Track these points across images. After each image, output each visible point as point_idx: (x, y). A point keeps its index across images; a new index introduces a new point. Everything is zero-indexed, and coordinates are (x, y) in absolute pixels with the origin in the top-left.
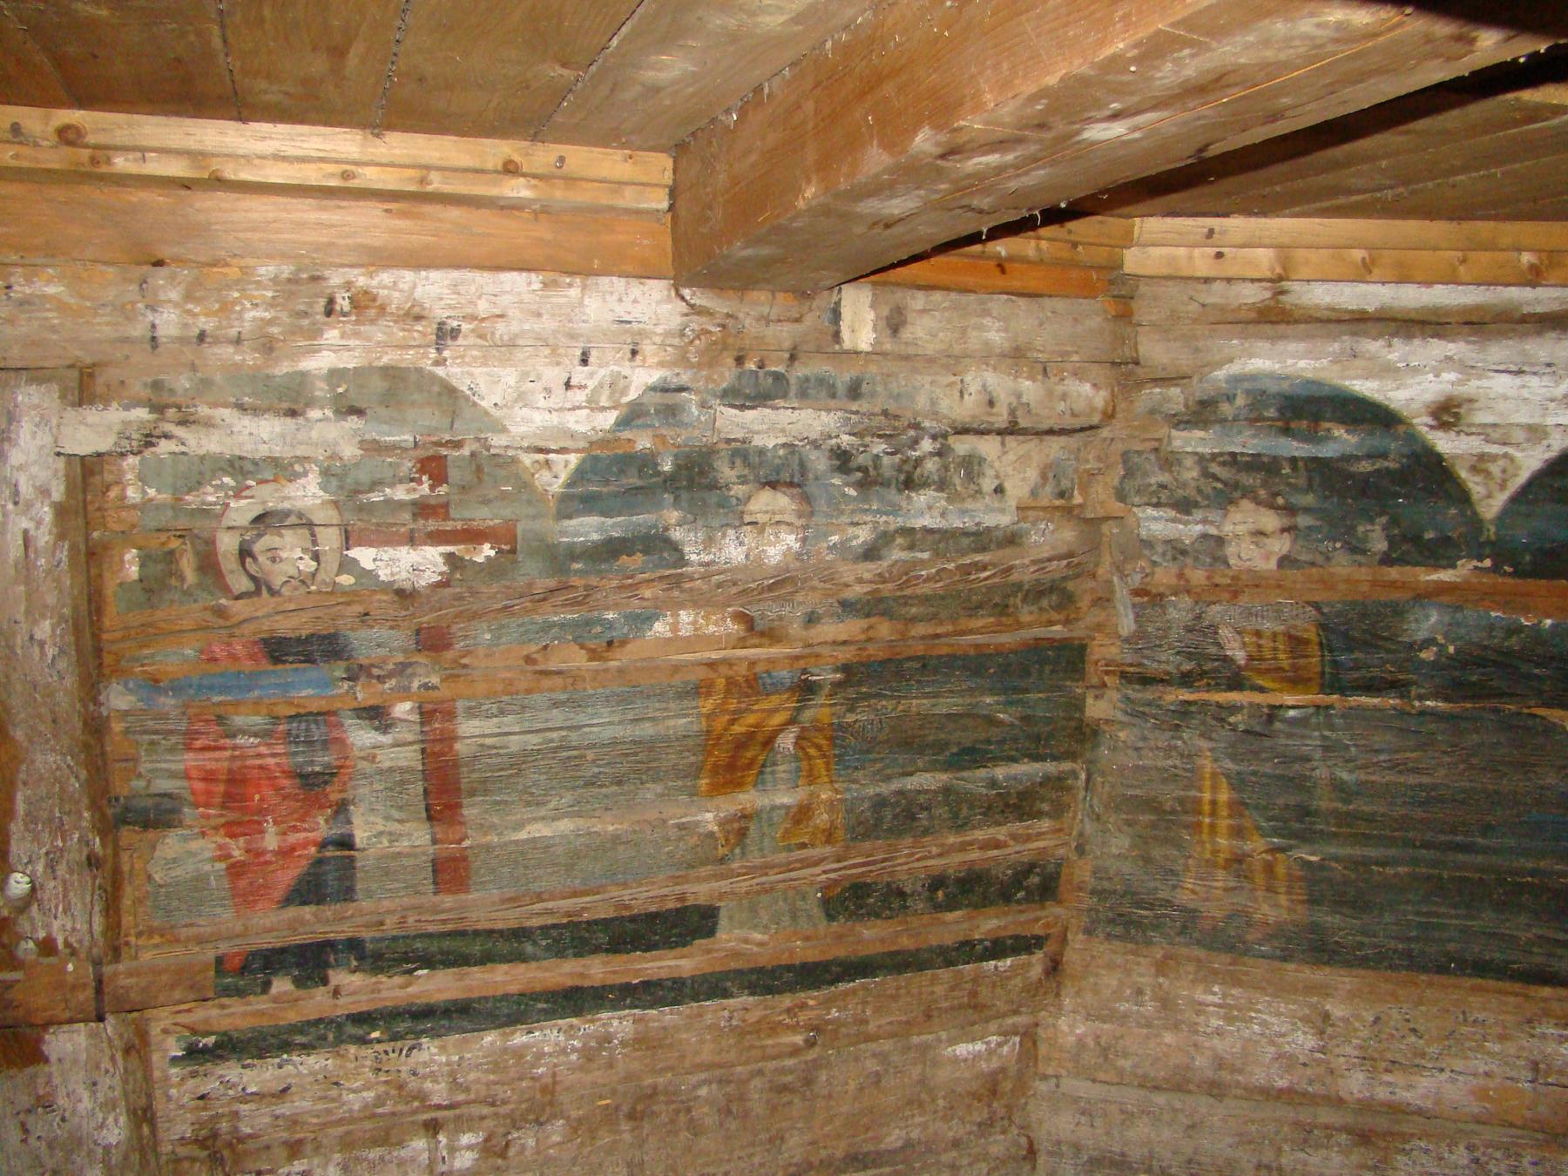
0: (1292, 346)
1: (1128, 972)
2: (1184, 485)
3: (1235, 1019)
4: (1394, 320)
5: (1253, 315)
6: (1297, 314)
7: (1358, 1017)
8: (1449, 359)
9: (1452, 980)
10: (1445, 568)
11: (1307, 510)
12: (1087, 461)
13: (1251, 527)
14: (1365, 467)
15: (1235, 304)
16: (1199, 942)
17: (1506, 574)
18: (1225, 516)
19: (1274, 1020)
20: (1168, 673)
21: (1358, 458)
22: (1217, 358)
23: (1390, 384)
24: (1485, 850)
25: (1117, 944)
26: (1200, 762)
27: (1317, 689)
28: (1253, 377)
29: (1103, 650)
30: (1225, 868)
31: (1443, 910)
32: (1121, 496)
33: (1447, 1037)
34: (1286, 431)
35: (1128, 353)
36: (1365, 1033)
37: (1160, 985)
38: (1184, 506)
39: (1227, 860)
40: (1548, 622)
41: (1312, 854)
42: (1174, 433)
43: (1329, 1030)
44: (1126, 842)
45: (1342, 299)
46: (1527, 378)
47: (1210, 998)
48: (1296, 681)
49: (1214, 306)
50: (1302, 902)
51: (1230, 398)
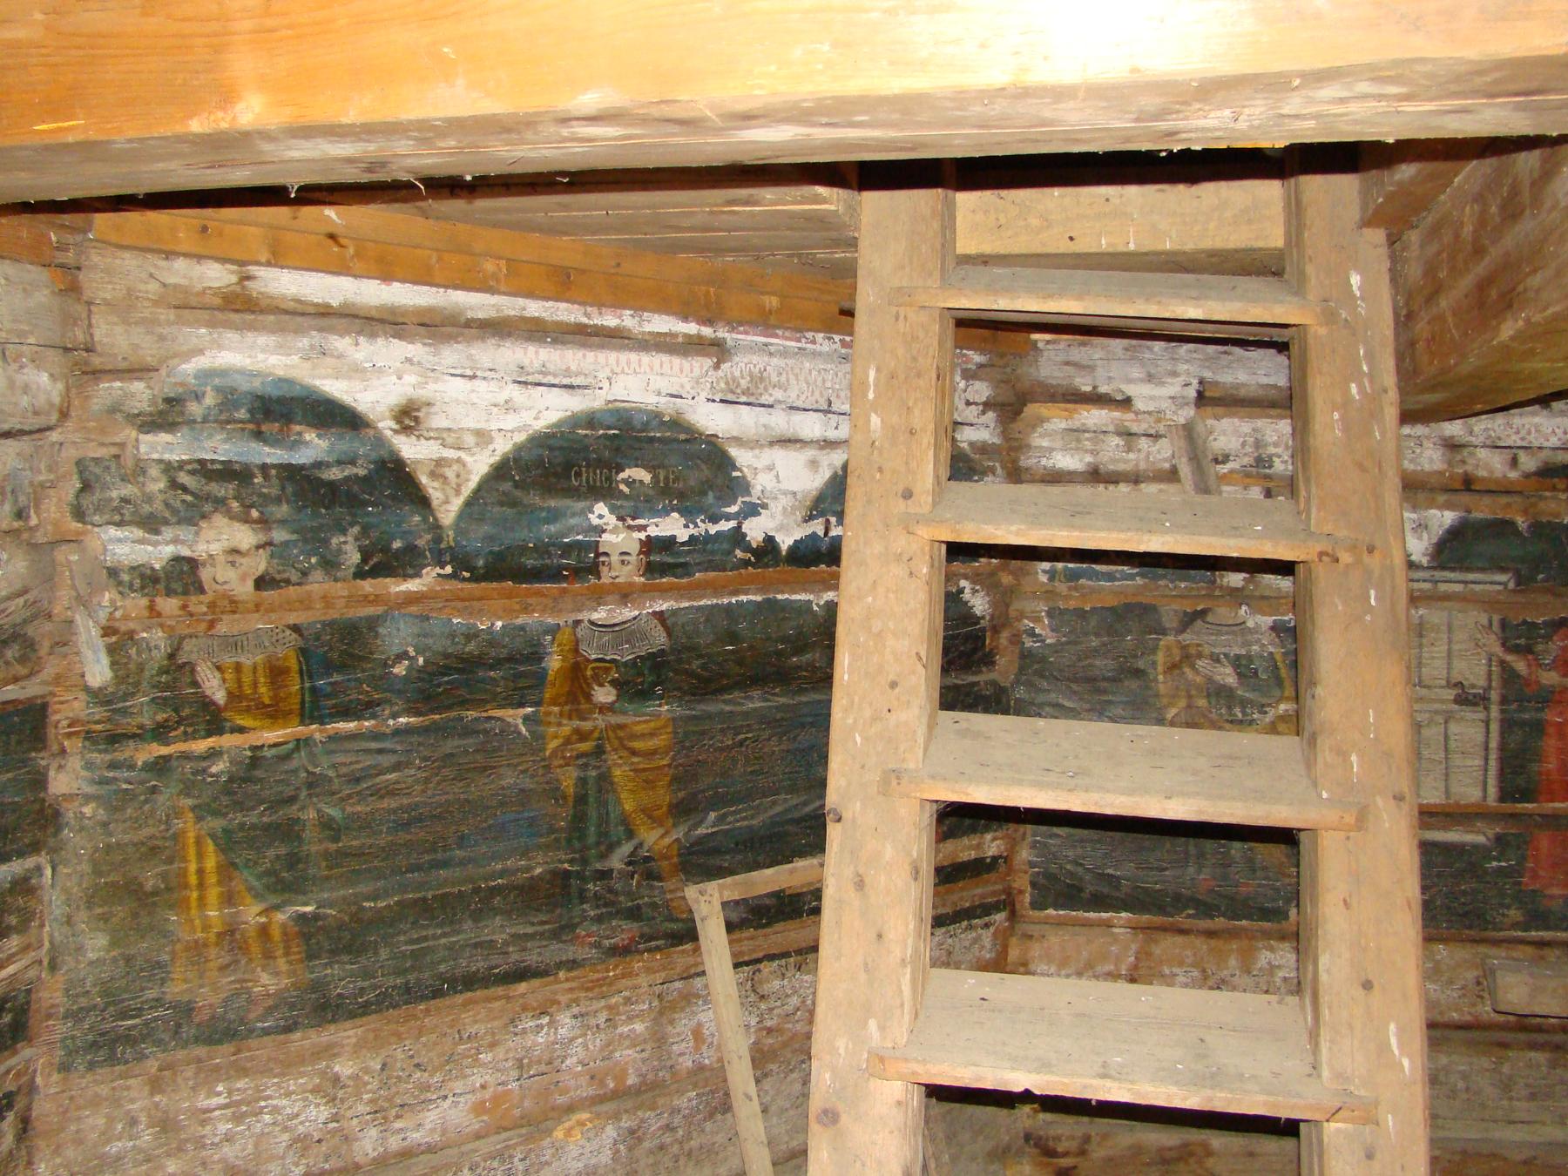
0: (262, 340)
1: (117, 1102)
2: (149, 499)
3: (244, 1115)
4: (356, 316)
5: (218, 301)
6: (264, 303)
7: (366, 1070)
8: (409, 360)
9: (447, 1001)
10: (412, 577)
11: (283, 522)
12: (39, 472)
13: (226, 545)
14: (335, 474)
15: (199, 287)
16: (197, 1040)
17: (464, 579)
18: (197, 534)
19: (285, 1102)
20: (141, 727)
21: (328, 465)
22: (184, 348)
23: (358, 385)
24: (463, 863)
25: (102, 1071)
26: (178, 824)
27: (297, 720)
28: (223, 373)
29: (70, 709)
30: (217, 944)
31: (430, 932)
32: (79, 514)
33: (448, 1062)
34: (258, 435)
35: (81, 336)
36: (375, 1084)
37: (157, 1105)
38: (152, 524)
39: (219, 935)
40: (499, 624)
41: (306, 904)
42: (142, 437)
43: (340, 1094)
44: (102, 940)
45: (308, 291)
46: (476, 382)
47: (215, 1101)
48: (273, 713)
49: (175, 286)
50: (302, 961)
51: (198, 397)
